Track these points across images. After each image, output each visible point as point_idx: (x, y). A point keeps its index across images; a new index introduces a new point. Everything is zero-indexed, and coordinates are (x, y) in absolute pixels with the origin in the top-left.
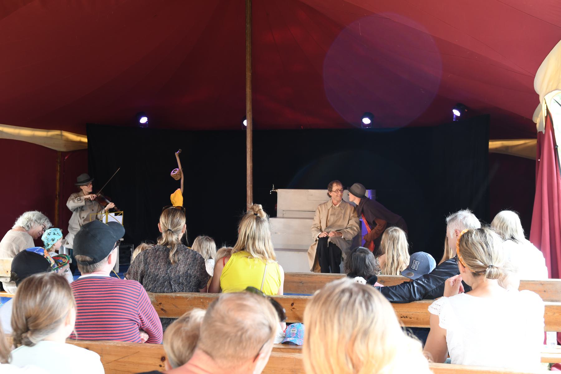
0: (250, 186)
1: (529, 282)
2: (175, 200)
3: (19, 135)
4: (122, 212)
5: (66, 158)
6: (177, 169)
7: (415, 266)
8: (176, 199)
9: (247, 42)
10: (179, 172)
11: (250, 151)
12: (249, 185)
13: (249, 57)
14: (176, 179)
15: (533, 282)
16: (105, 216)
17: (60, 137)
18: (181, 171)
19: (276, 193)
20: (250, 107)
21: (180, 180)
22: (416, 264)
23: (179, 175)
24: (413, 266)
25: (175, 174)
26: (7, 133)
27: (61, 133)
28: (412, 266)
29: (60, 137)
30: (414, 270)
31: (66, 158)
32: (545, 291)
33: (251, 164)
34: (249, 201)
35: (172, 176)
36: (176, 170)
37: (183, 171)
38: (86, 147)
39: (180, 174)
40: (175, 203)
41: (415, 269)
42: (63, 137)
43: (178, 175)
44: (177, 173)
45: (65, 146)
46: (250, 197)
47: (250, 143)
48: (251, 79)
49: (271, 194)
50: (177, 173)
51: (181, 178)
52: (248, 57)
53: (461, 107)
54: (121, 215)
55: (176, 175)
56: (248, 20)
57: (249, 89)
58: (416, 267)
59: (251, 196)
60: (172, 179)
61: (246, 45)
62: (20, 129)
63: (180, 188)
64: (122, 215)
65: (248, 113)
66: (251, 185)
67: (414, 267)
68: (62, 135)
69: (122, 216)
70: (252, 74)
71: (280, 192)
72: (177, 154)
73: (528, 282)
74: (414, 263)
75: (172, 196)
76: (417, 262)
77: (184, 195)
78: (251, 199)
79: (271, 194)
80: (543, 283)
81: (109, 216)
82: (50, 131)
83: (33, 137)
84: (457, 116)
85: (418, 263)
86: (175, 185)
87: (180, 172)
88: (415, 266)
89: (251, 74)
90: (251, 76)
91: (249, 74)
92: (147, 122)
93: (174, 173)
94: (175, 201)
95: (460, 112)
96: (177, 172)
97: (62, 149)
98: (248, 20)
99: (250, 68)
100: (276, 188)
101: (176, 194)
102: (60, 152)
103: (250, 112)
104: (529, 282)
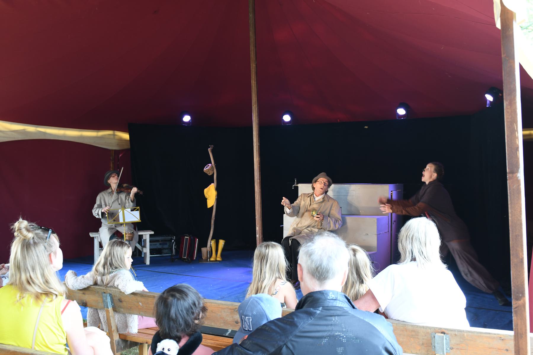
0: (258, 182)
1: (482, 335)
2: (209, 194)
3: (64, 136)
4: (139, 207)
5: (120, 155)
6: (210, 165)
7: (247, 324)
8: (209, 194)
9: (250, 32)
10: (211, 167)
11: (257, 145)
12: (257, 181)
13: (252, 48)
14: (209, 175)
15: (488, 335)
16: (122, 212)
17: (112, 137)
18: (214, 166)
19: (297, 187)
20: (255, 99)
21: (213, 174)
22: (248, 322)
23: (211, 171)
24: (245, 325)
25: (207, 170)
26: (50, 134)
27: (114, 133)
28: (244, 326)
29: (112, 137)
30: (248, 331)
31: (120, 155)
32: (507, 350)
33: (258, 159)
34: (256, 197)
35: (205, 171)
36: (209, 166)
37: (216, 166)
38: (128, 146)
39: (212, 169)
40: (209, 197)
41: (250, 330)
42: (116, 137)
43: (210, 171)
44: (209, 168)
45: (118, 144)
46: (258, 193)
47: (256, 137)
48: (255, 71)
49: (293, 188)
50: (209, 168)
51: (214, 172)
52: (252, 48)
53: (494, 91)
54: (138, 210)
55: (208, 170)
56: (251, 9)
57: (253, 81)
58: (249, 326)
59: (259, 192)
60: (206, 174)
61: (250, 35)
62: (65, 130)
63: (213, 182)
64: (138, 210)
65: (253, 106)
66: (259, 181)
67: (247, 327)
68: (114, 135)
69: (138, 211)
70: (256, 65)
71: (300, 186)
72: (209, 150)
73: (480, 335)
74: (245, 321)
75: (206, 190)
76: (247, 318)
77: (217, 189)
78: (258, 195)
79: (293, 188)
80: (503, 338)
81: (125, 211)
82: (100, 132)
83: (82, 137)
84: (490, 102)
85: (249, 319)
86: (208, 181)
87: (212, 167)
88: (247, 324)
89: (255, 66)
90: (255, 67)
91: (253, 66)
92: (190, 120)
93: (206, 169)
94: (208, 196)
95: (493, 96)
96: (209, 167)
97: (114, 147)
98: (251, 9)
99: (255, 59)
100: (297, 184)
101: (209, 189)
102: (112, 150)
103: (255, 104)
104: (482, 335)
